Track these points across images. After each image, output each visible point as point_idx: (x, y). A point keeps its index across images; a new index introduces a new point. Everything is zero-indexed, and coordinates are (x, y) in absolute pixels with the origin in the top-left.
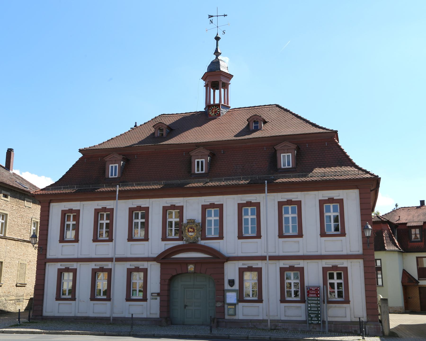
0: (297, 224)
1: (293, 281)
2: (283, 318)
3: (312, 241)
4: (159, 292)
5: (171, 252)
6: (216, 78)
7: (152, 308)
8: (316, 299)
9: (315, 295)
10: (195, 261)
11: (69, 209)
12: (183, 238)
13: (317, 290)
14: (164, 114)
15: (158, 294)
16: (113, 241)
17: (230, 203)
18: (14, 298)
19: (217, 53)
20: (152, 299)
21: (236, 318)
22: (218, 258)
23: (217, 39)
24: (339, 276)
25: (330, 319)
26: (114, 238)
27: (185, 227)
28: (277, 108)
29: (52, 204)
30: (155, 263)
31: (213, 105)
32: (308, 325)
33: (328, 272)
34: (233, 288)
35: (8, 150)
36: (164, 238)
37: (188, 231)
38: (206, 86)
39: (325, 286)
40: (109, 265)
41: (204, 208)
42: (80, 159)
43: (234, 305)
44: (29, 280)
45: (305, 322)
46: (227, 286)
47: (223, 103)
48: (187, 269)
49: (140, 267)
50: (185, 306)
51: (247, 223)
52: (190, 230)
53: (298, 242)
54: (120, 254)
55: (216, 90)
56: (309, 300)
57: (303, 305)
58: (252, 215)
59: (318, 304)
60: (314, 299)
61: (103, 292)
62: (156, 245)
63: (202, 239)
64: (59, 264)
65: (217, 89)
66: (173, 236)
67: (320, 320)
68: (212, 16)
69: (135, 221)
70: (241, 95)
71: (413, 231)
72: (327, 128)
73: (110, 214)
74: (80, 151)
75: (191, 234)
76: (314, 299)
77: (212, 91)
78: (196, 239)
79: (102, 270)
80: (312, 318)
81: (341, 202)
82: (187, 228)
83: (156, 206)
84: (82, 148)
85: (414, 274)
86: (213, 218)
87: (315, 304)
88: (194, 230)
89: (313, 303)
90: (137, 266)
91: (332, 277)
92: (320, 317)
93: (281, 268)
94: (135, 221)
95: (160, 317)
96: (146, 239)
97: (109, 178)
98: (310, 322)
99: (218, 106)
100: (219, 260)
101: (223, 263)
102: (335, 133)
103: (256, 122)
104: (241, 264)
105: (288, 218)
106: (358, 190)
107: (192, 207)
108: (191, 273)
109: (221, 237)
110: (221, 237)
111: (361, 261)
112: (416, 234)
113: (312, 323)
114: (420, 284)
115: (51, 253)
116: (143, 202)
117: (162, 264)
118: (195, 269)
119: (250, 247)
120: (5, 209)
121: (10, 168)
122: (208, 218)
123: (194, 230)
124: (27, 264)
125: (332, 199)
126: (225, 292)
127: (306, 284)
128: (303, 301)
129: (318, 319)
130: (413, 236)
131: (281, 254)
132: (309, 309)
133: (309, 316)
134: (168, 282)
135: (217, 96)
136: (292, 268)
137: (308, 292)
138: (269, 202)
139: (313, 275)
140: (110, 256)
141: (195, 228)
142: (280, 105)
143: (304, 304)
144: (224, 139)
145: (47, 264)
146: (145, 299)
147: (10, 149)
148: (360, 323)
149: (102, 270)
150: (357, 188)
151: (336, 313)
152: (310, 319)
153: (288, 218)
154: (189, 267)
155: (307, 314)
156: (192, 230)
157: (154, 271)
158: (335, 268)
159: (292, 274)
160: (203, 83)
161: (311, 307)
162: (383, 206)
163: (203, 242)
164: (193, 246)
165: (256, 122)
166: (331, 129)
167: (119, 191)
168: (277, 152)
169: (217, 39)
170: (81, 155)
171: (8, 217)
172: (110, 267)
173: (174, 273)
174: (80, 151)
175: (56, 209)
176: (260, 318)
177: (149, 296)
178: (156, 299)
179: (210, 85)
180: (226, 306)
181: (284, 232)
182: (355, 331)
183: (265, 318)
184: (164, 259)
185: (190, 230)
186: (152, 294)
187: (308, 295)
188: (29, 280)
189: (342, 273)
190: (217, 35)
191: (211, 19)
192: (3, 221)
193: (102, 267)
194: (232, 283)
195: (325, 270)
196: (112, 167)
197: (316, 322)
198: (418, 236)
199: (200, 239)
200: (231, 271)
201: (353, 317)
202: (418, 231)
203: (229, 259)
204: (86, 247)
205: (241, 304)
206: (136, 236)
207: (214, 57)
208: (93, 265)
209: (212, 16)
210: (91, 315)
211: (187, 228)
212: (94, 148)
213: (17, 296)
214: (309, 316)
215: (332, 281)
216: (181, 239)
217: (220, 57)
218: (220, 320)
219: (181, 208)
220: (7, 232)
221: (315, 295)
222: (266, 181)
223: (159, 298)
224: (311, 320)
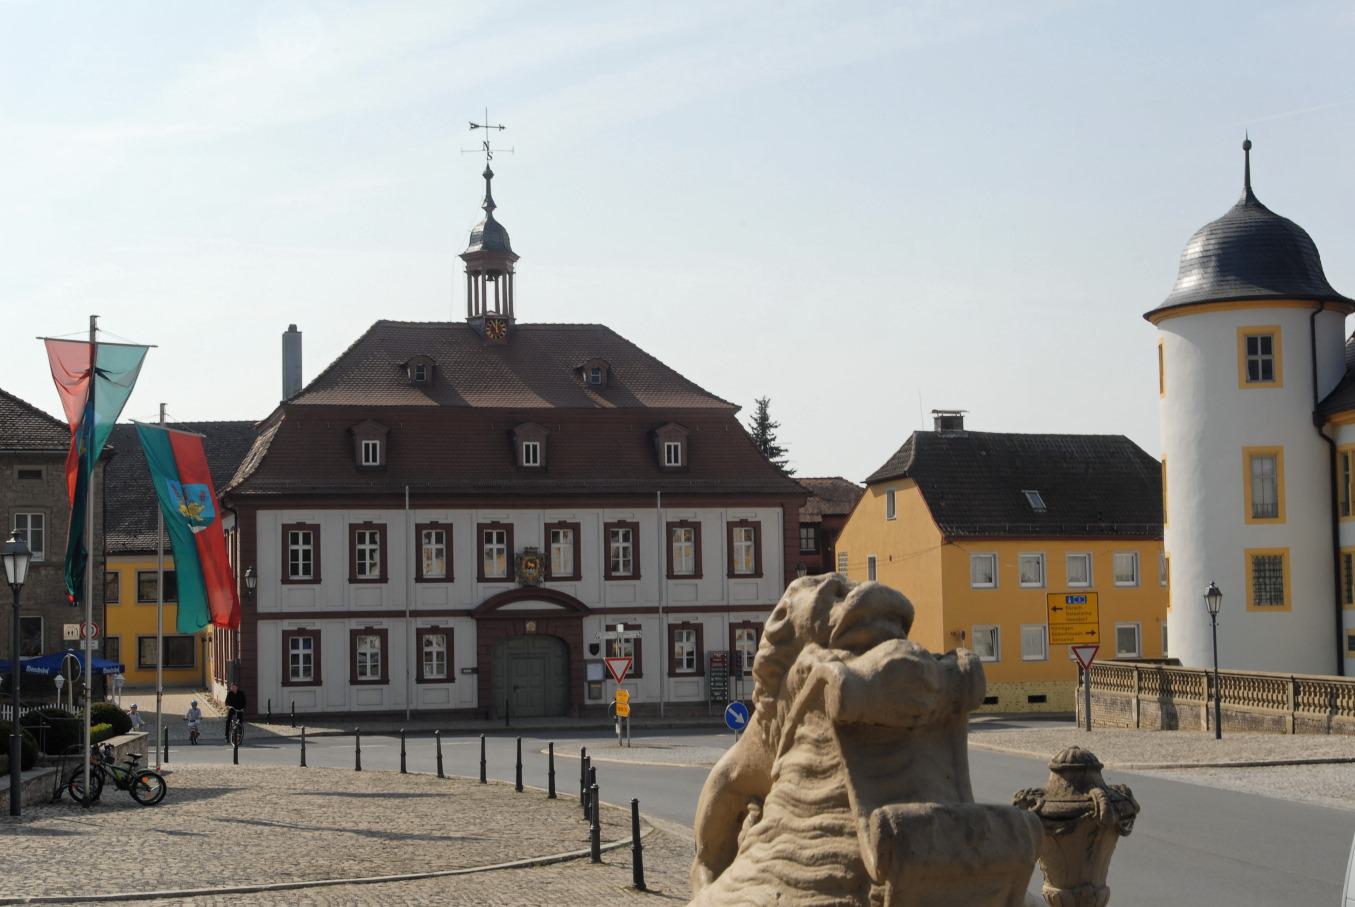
1: (434, 649)
4: (475, 666)
6: (491, 255)
7: (463, 692)
15: (474, 671)
17: (592, 521)
22: (578, 610)
23: (488, 175)
30: (468, 619)
33: (290, 638)
34: (597, 657)
37: (527, 566)
46: (587, 655)
48: (525, 628)
49: (375, 627)
50: (516, 688)
52: (530, 564)
53: (380, 588)
57: (700, 679)
61: (682, 665)
62: (467, 592)
63: (546, 580)
68: (476, 126)
70: (540, 298)
74: (1164, 461)
82: (524, 562)
83: (465, 522)
90: (436, 624)
94: (487, 547)
95: (479, 706)
96: (449, 578)
97: (362, 466)
100: (576, 610)
101: (580, 619)
102: (950, 422)
107: (528, 526)
108: (530, 634)
110: (576, 576)
115: (264, 604)
116: (375, 516)
117: (478, 620)
118: (537, 627)
128: (700, 673)
131: (286, 609)
133: (712, 695)
136: (435, 630)
137: (711, 660)
138: (651, 521)
140: (402, 608)
143: (702, 678)
146: (451, 679)
154: (528, 626)
156: (533, 565)
157: (466, 635)
159: (433, 638)
160: (463, 265)
161: (715, 682)
163: (549, 585)
164: (530, 592)
169: (488, 175)
174: (1164, 461)
180: (586, 685)
184: (486, 616)
186: (463, 669)
192: (442, 546)
193: (368, 627)
195: (286, 634)
196: (676, 461)
199: (542, 579)
200: (593, 631)
204: (334, 588)
209: (476, 126)
210: (355, 708)
211: (524, 562)
214: (712, 695)
216: (509, 578)
217: (496, 215)
221: (720, 665)
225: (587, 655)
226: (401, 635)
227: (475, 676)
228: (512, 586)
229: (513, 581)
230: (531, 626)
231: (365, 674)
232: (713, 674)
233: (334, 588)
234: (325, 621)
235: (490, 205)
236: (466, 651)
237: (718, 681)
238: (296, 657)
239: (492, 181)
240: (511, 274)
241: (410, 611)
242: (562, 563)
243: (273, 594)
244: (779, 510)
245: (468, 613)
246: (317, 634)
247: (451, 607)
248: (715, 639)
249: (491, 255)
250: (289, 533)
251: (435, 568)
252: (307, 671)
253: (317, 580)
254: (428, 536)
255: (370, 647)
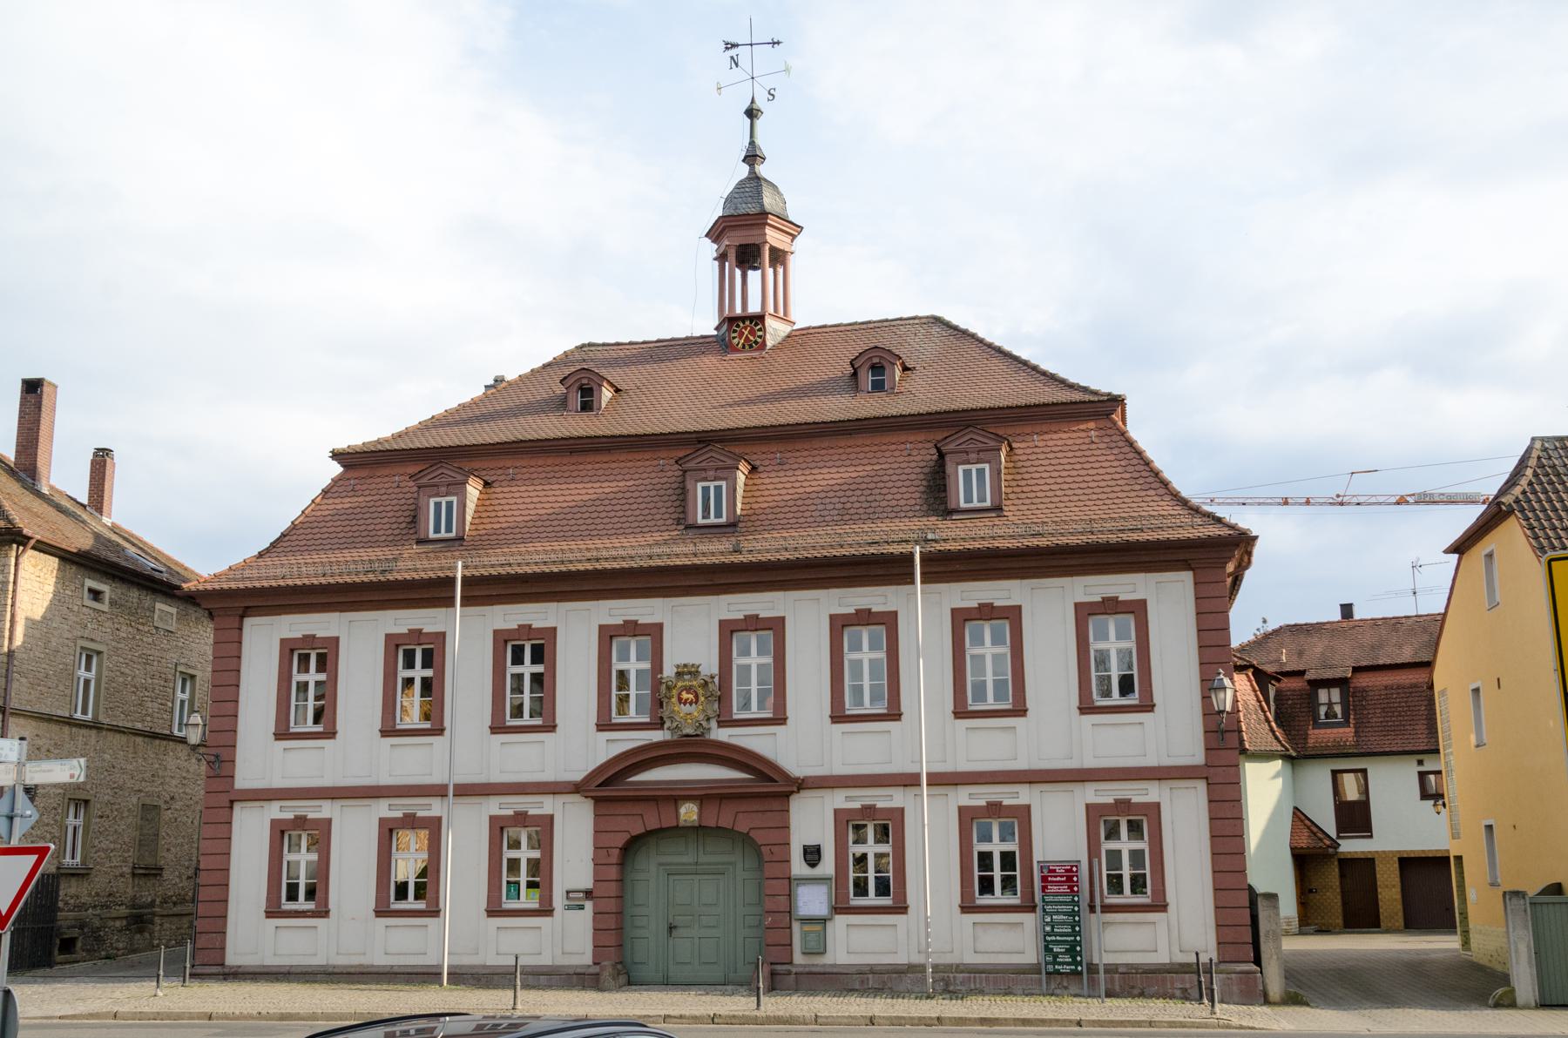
0: (1009, 677)
2: (970, 959)
3: (1054, 730)
5: (735, 756)
6: (746, 234)
8: (1068, 899)
9: (1064, 889)
10: (707, 795)
11: (858, 611)
12: (663, 724)
13: (1070, 876)
14: (590, 345)
15: (588, 894)
16: (447, 733)
18: (123, 911)
19: (752, 157)
20: (569, 908)
21: (828, 960)
23: (752, 113)
24: (1135, 829)
25: (1109, 959)
26: (447, 723)
27: (669, 688)
28: (936, 329)
29: (249, 622)
30: (576, 798)
31: (743, 319)
32: (1044, 976)
35: (95, 455)
36: (604, 725)
37: (680, 700)
38: (722, 258)
39: (1096, 861)
40: (435, 808)
41: (728, 630)
42: (335, 481)
43: (823, 921)
44: (170, 856)
45: (1035, 969)
46: (798, 867)
47: (771, 310)
50: (671, 928)
51: (857, 674)
52: (685, 695)
54: (468, 773)
55: (750, 273)
56: (1047, 903)
57: (1029, 919)
58: (872, 648)
59: (1073, 914)
60: (1061, 899)
62: (578, 745)
64: (276, 805)
65: (755, 268)
66: (632, 716)
67: (1080, 963)
68: (734, 46)
69: (298, 677)
70: (832, 285)
71: (1323, 695)
72: (1093, 387)
73: (432, 651)
74: (337, 455)
75: (686, 709)
76: (1061, 899)
77: (738, 272)
78: (704, 723)
79: (411, 822)
80: (1056, 956)
81: (1138, 609)
83: (576, 628)
84: (342, 444)
85: (1327, 821)
86: (753, 658)
87: (1065, 914)
88: (697, 696)
89: (1058, 913)
90: (520, 808)
91: (1113, 834)
92: (1080, 954)
93: (962, 810)
98: (1050, 968)
99: (759, 319)
100: (772, 787)
103: (877, 369)
104: (840, 799)
105: (860, 662)
106: (1190, 574)
107: (691, 631)
109: (779, 719)
110: (779, 719)
111: (1201, 786)
112: (1330, 704)
113: (1058, 972)
114: (1341, 849)
115: (247, 775)
116: (425, 619)
117: (598, 801)
118: (700, 815)
119: (862, 749)
120: (97, 636)
121: (105, 508)
122: (738, 661)
123: (697, 696)
124: (164, 806)
125: (990, 606)
126: (794, 883)
127: (1038, 856)
129: (1074, 958)
130: (1323, 710)
132: (1048, 929)
133: (1048, 950)
134: (622, 856)
135: (755, 289)
137: (1044, 879)
139: (1059, 831)
140: (436, 779)
141: (700, 691)
142: (947, 318)
144: (782, 421)
145: (237, 807)
146: (546, 911)
147: (103, 450)
148: (1193, 969)
149: (411, 822)
150: (1189, 568)
151: (1121, 940)
152: (1050, 959)
153: (749, 667)
154: (683, 810)
155: (1042, 945)
158: (1123, 805)
160: (711, 249)
162: (1247, 620)
163: (722, 735)
165: (877, 369)
166: (1105, 390)
167: (464, 578)
168: (948, 458)
170: (336, 469)
171: (106, 663)
172: (434, 813)
173: (638, 829)
174: (337, 455)
175: (263, 639)
176: (901, 959)
177: (558, 900)
178: (581, 907)
179: (732, 256)
180: (796, 926)
181: (970, 701)
182: (1184, 990)
183: (916, 959)
184: (607, 787)
185: (685, 695)
187: (1044, 888)
188: (170, 856)
189: (1144, 820)
190: (753, 101)
191: (733, 52)
193: (410, 815)
194: (812, 855)
195: (1093, 812)
196: (438, 505)
197: (1067, 969)
198: (1338, 709)
199: (714, 724)
200: (811, 821)
201: (1176, 949)
202: (1336, 694)
203: (802, 785)
204: (359, 750)
205: (841, 920)
206: (407, 719)
207: (744, 170)
208: (384, 809)
209: (734, 46)
212: (380, 447)
213: (133, 907)
215: (1112, 845)
216: (658, 724)
217: (763, 170)
218: (779, 967)
219: (655, 632)
220: (102, 709)
221: (1064, 889)
222: (460, 564)
223: (589, 905)
224: (1055, 963)
225: (798, 867)
226: (354, 834)
227: (589, 905)
228: (657, 736)
229: (662, 728)
230: (689, 813)
231: (891, 892)
232: (1048, 908)
233: (359, 750)
234: (1037, 788)
235: (752, 157)
236: (575, 860)
237: (1063, 923)
238: (514, 865)
239: (759, 123)
240: (779, 257)
241: (456, 786)
242: (750, 692)
243: (260, 758)
244: (1187, 577)
245: (576, 788)
246: (1024, 813)
247: (548, 776)
248: (1059, 831)
249: (746, 234)
250: (294, 653)
251: (412, 708)
252: (1008, 883)
253: (551, 727)
254: (304, 659)
255: (302, 858)
